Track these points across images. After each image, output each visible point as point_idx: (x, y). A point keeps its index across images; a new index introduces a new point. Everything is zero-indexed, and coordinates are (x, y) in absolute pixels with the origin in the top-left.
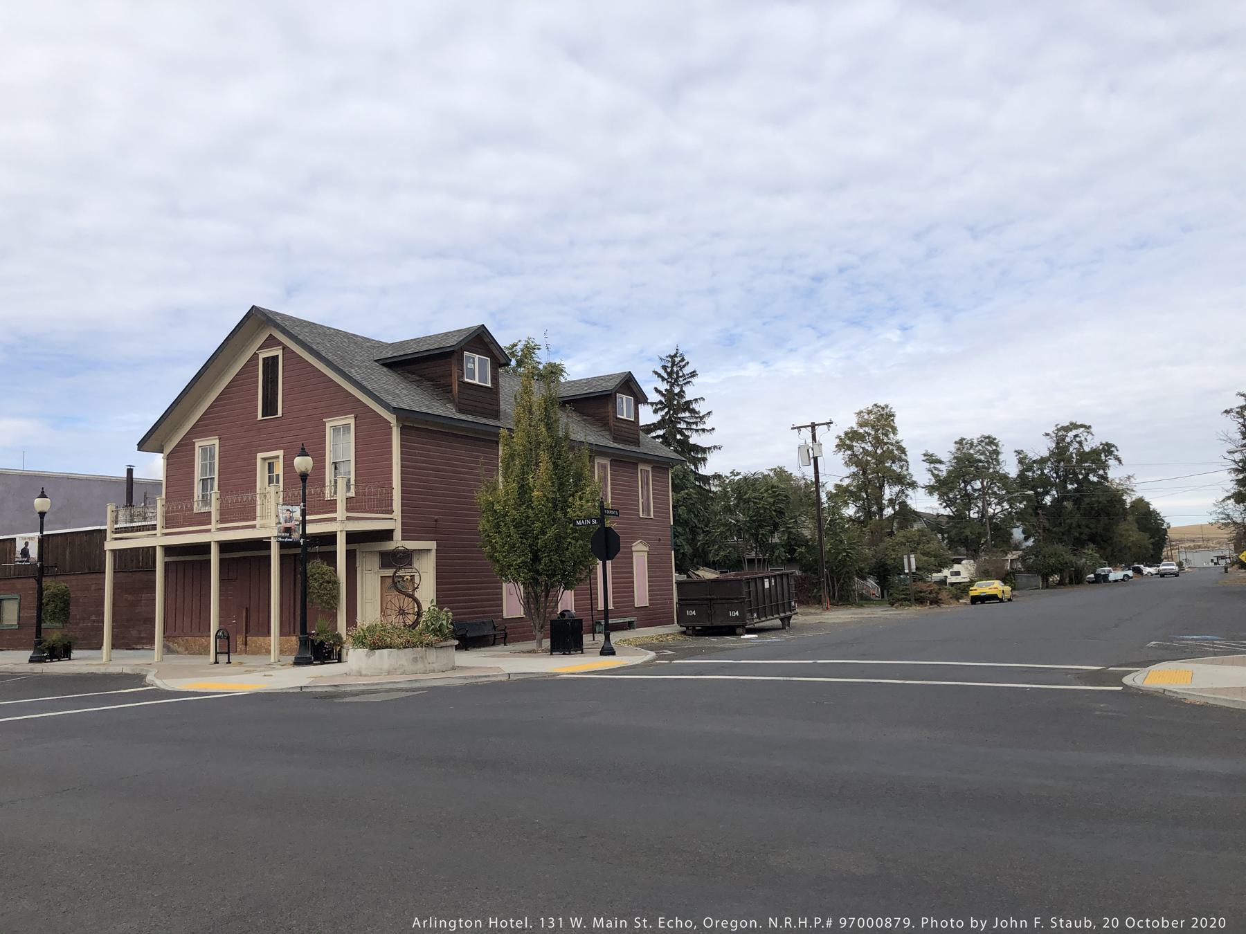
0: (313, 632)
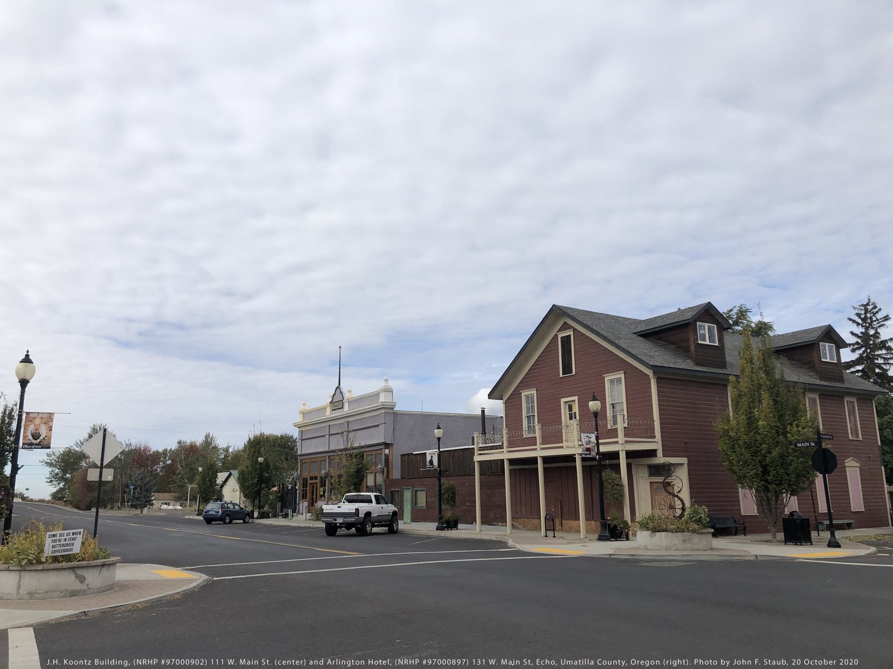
0: (609, 518)
